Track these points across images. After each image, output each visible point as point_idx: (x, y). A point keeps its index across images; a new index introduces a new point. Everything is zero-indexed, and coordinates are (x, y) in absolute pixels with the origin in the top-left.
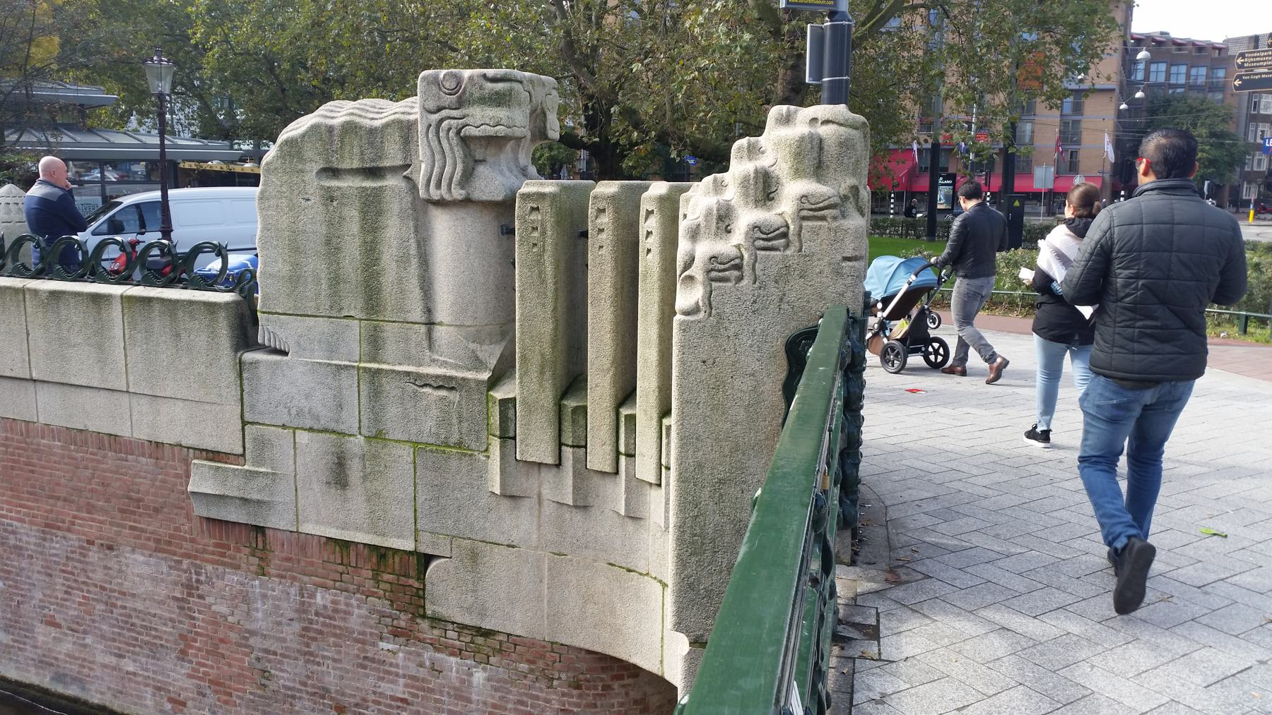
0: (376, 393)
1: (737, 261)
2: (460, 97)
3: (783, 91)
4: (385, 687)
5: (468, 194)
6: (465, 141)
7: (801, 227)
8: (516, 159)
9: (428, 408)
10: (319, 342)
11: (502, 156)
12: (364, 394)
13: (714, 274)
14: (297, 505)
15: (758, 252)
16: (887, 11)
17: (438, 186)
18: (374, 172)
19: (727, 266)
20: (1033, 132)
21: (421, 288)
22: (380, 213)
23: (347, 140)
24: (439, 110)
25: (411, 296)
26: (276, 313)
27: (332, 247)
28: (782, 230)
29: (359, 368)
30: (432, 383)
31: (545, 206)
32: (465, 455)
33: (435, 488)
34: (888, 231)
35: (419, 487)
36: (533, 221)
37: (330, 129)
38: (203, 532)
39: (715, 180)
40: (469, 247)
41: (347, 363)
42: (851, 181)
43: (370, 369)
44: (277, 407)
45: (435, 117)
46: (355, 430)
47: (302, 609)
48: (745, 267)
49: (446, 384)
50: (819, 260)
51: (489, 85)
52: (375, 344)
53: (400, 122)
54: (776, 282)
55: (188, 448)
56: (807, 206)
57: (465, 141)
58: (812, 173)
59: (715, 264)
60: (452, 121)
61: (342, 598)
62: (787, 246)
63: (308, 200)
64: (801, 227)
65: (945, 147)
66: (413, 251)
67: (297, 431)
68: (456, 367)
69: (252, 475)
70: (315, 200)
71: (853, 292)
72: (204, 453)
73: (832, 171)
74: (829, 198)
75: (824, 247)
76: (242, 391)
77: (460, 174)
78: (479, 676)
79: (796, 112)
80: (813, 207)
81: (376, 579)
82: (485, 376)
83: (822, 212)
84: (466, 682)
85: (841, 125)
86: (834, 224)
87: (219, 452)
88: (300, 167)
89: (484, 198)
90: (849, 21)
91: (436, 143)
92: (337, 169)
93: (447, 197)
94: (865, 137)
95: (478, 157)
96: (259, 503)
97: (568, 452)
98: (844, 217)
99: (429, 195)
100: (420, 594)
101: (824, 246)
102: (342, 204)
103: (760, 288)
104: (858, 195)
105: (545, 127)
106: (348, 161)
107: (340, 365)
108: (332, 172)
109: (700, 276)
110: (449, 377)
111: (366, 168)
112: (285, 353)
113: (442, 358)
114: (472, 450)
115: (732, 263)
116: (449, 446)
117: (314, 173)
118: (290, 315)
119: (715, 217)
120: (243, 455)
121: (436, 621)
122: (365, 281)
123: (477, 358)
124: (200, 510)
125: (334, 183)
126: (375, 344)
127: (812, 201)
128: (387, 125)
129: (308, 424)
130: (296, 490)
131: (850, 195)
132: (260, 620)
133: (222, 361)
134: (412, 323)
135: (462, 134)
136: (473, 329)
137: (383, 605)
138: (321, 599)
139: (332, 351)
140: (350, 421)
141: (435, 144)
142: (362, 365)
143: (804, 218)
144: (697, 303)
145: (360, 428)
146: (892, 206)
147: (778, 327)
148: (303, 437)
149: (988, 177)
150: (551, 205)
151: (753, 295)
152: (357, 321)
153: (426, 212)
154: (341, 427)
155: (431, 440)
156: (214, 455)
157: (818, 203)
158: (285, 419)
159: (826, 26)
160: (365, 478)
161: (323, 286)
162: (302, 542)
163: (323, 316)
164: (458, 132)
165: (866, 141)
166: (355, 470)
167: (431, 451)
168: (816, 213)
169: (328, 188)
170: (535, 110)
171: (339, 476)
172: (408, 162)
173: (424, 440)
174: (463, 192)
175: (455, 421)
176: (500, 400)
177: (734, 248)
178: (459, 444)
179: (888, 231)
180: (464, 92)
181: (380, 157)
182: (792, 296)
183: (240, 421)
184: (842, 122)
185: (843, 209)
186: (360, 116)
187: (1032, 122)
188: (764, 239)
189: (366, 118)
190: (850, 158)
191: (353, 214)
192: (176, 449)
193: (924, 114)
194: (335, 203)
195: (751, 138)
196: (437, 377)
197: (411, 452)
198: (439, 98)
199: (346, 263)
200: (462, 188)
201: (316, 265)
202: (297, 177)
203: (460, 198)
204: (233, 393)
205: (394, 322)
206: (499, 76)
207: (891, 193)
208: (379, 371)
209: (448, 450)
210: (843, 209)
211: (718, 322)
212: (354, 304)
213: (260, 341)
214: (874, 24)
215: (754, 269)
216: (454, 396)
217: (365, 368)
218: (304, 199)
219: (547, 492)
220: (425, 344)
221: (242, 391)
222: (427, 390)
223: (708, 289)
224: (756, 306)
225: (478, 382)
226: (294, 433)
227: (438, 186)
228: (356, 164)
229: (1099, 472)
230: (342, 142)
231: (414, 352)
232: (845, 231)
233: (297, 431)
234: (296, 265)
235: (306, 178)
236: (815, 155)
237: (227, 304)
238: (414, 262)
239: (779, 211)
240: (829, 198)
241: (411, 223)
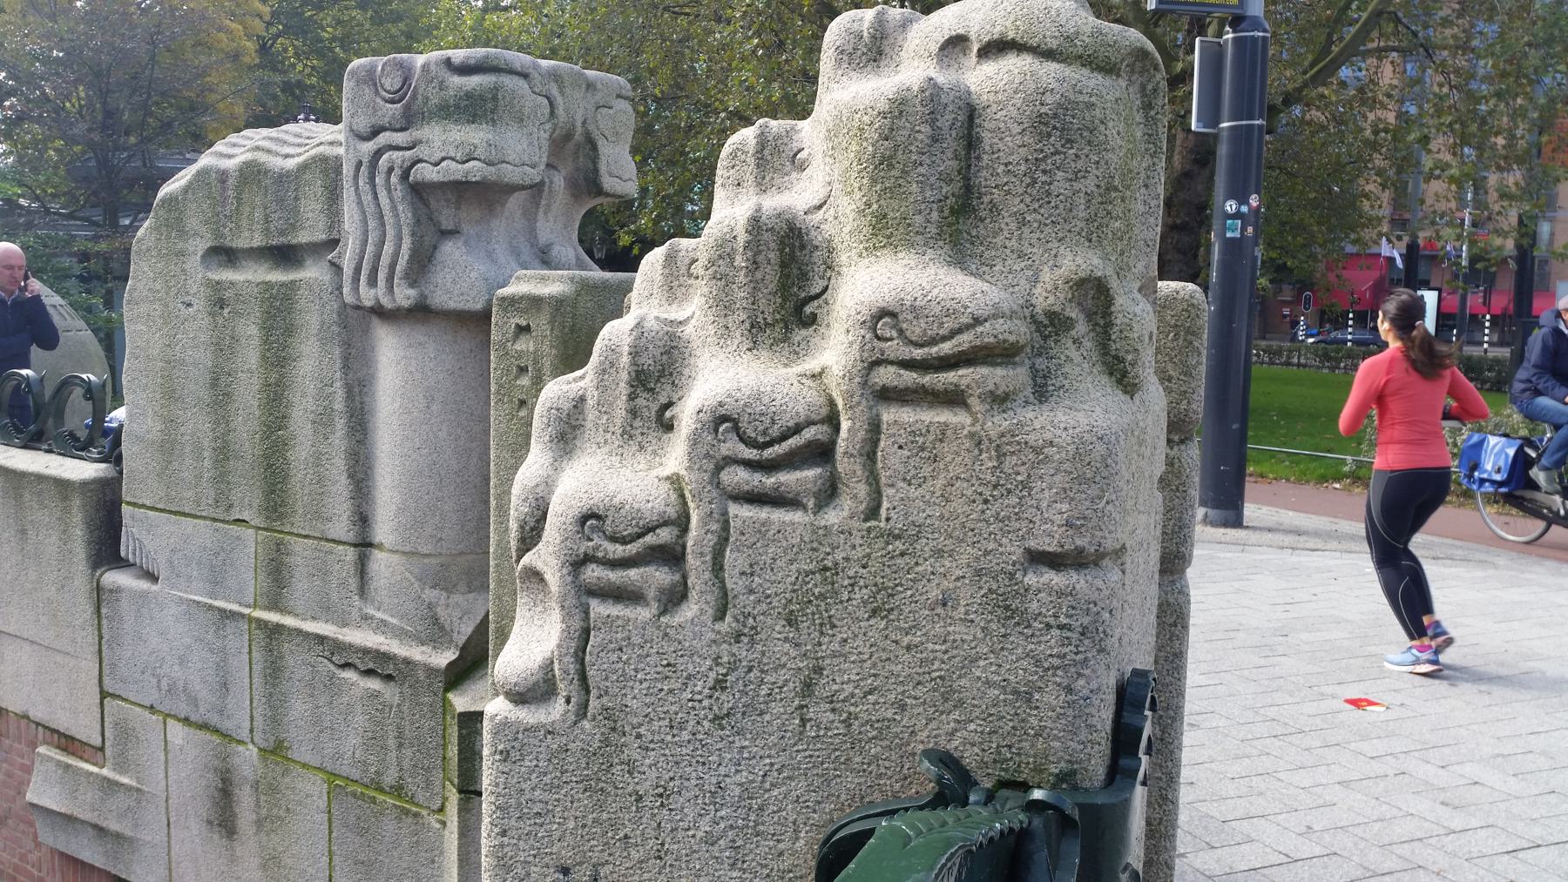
0: (274, 671)
1: (665, 535)
2: (407, 108)
3: (1182, 163)
5: (423, 296)
6: (419, 192)
7: (875, 428)
8: (532, 232)
9: (349, 711)
10: (199, 563)
11: (495, 223)
12: (257, 668)
13: (593, 573)
14: (169, 851)
15: (734, 509)
16: (1341, 53)
17: (372, 282)
18: (285, 255)
19: (632, 549)
20: (1552, 234)
21: (350, 476)
22: (290, 331)
23: (245, 196)
24: (375, 132)
25: (334, 489)
26: (143, 506)
28: (809, 434)
29: (250, 619)
30: (357, 662)
31: (541, 323)
32: (407, 812)
33: (360, 867)
34: (1342, 365)
35: (336, 859)
36: (520, 355)
37: (223, 175)
38: (54, 869)
39: (670, 259)
40: (430, 400)
41: (235, 607)
42: (1077, 261)
43: (266, 623)
44: (143, 673)
45: (369, 147)
46: (244, 734)
48: (692, 561)
49: (379, 666)
50: (939, 553)
51: (456, 80)
52: (277, 573)
53: (324, 159)
54: (791, 621)
55: (38, 724)
56: (896, 349)
57: (419, 192)
58: (933, 230)
59: (597, 540)
60: (396, 155)
62: (829, 492)
63: (189, 305)
64: (875, 428)
65: (1427, 253)
66: (339, 405)
67: (168, 720)
68: (401, 634)
69: (110, 786)
70: (199, 305)
71: (1069, 690)
72: (56, 736)
73: (1008, 222)
74: (977, 321)
75: (958, 505)
76: (101, 637)
77: (406, 257)
79: (905, 25)
80: (918, 353)
82: (443, 658)
83: (950, 377)
85: (1048, 54)
86: (998, 423)
87: (72, 739)
88: (180, 246)
89: (452, 305)
90: (1265, 31)
91: (370, 197)
92: (231, 249)
93: (386, 302)
94: (1147, 106)
95: (447, 224)
96: (118, 836)
98: (1042, 392)
99: (359, 299)
101: (958, 505)
102: (234, 312)
103: (738, 637)
104: (1107, 314)
105: (596, 170)
106: (247, 234)
107: (225, 611)
108: (224, 254)
109: (554, 577)
110: (384, 654)
111: (272, 246)
113: (379, 615)
114: (417, 805)
115: (649, 539)
116: (381, 790)
117: (198, 258)
118: (162, 511)
119: (624, 376)
120: (102, 749)
122: (266, 457)
123: (436, 620)
124: (50, 837)
125: (228, 275)
127: (915, 330)
128: (304, 167)
129: (183, 709)
130: (169, 825)
131: (1073, 313)
133: (76, 583)
134: (334, 541)
135: (411, 179)
136: (434, 561)
139: (216, 582)
141: (367, 198)
142: (258, 614)
143: (887, 395)
144: (548, 666)
145: (251, 731)
146: (1350, 330)
147: (799, 787)
148: (177, 732)
149: (1487, 294)
150: (552, 322)
151: (717, 660)
152: (251, 531)
153: (366, 331)
154: (226, 725)
155: (355, 774)
156: (68, 743)
157: (933, 341)
159: (1227, 39)
160: (259, 823)
161: (206, 463)
163: (204, 518)
164: (405, 176)
165: (1150, 121)
167: (354, 795)
168: (927, 379)
169: (218, 283)
170: (568, 136)
172: (335, 235)
173: (345, 770)
174: (412, 292)
175: (391, 742)
176: (461, 714)
177: (667, 485)
178: (398, 790)
179: (1342, 365)
180: (414, 97)
181: (293, 226)
182: (843, 679)
183: (98, 690)
184: (1053, 44)
185: (1041, 363)
186: (269, 151)
187: (1551, 220)
188: (750, 464)
189: (277, 154)
190: (1076, 176)
192: (23, 722)
193: (1397, 204)
194: (226, 311)
195: (773, 123)
196: (366, 651)
197: (325, 791)
198: (375, 111)
199: (238, 421)
200: (412, 285)
202: (176, 264)
203: (406, 304)
204: (90, 637)
205: (306, 537)
206: (472, 62)
207: (1349, 312)
208: (278, 629)
209: (381, 797)
210: (1041, 363)
211: (606, 742)
212: (248, 501)
213: (123, 554)
214: (1320, 71)
215: (717, 567)
216: (390, 692)
217: (259, 621)
218: (183, 303)
220: (353, 583)
221: (101, 637)
222: (349, 675)
223: (577, 624)
224: (727, 700)
225: (431, 671)
226: (165, 723)
227: (372, 282)
228: (257, 241)
230: (239, 199)
231: (334, 596)
232: (1037, 451)
233: (168, 720)
234: (170, 422)
235: (187, 266)
236: (950, 165)
237: (84, 484)
238: (340, 424)
239: (812, 364)
240: (977, 321)
241: (337, 351)
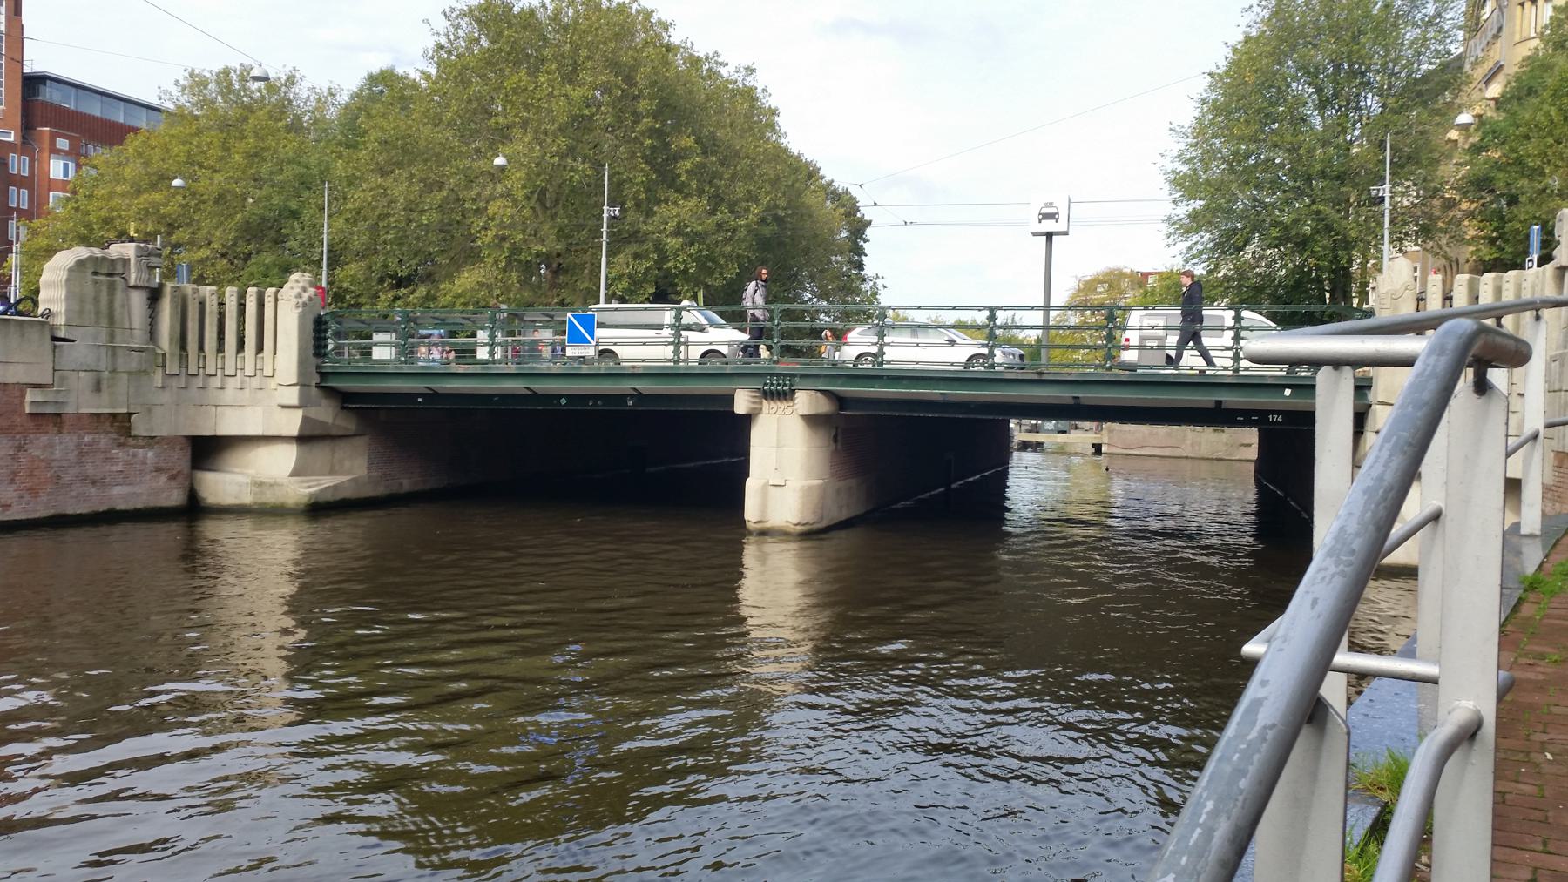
4: (114, 468)
27: (96, 300)
47: (78, 445)
49: (140, 350)
52: (112, 337)
61: (97, 436)
69: (59, 392)
78: (150, 454)
81: (112, 426)
84: (145, 457)
96: (62, 403)
97: (239, 371)
100: (129, 428)
108: (95, 273)
112: (73, 341)
121: (135, 437)
126: (112, 337)
132: (58, 454)
137: (114, 436)
138: (87, 439)
140: (103, 365)
148: (82, 374)
158: (74, 367)
160: (109, 387)
162: (79, 416)
166: (104, 385)
171: (98, 387)
191: (104, 289)
201: (89, 307)
212: (104, 322)
216: (144, 354)
219: (174, 384)
229: (818, 394)
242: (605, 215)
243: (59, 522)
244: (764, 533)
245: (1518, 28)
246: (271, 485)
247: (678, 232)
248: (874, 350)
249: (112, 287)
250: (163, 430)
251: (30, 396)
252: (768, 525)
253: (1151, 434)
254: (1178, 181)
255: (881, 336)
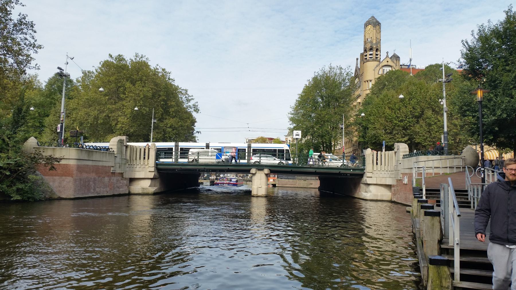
140: (121, 163)
242: (152, 122)
243: (114, 196)
244: (258, 197)
245: (364, 87)
246: (146, 189)
247: (170, 127)
248: (259, 161)
249: (122, 146)
250: (127, 177)
251: (112, 169)
252: (258, 195)
253: (288, 181)
254: (292, 119)
255: (260, 158)
